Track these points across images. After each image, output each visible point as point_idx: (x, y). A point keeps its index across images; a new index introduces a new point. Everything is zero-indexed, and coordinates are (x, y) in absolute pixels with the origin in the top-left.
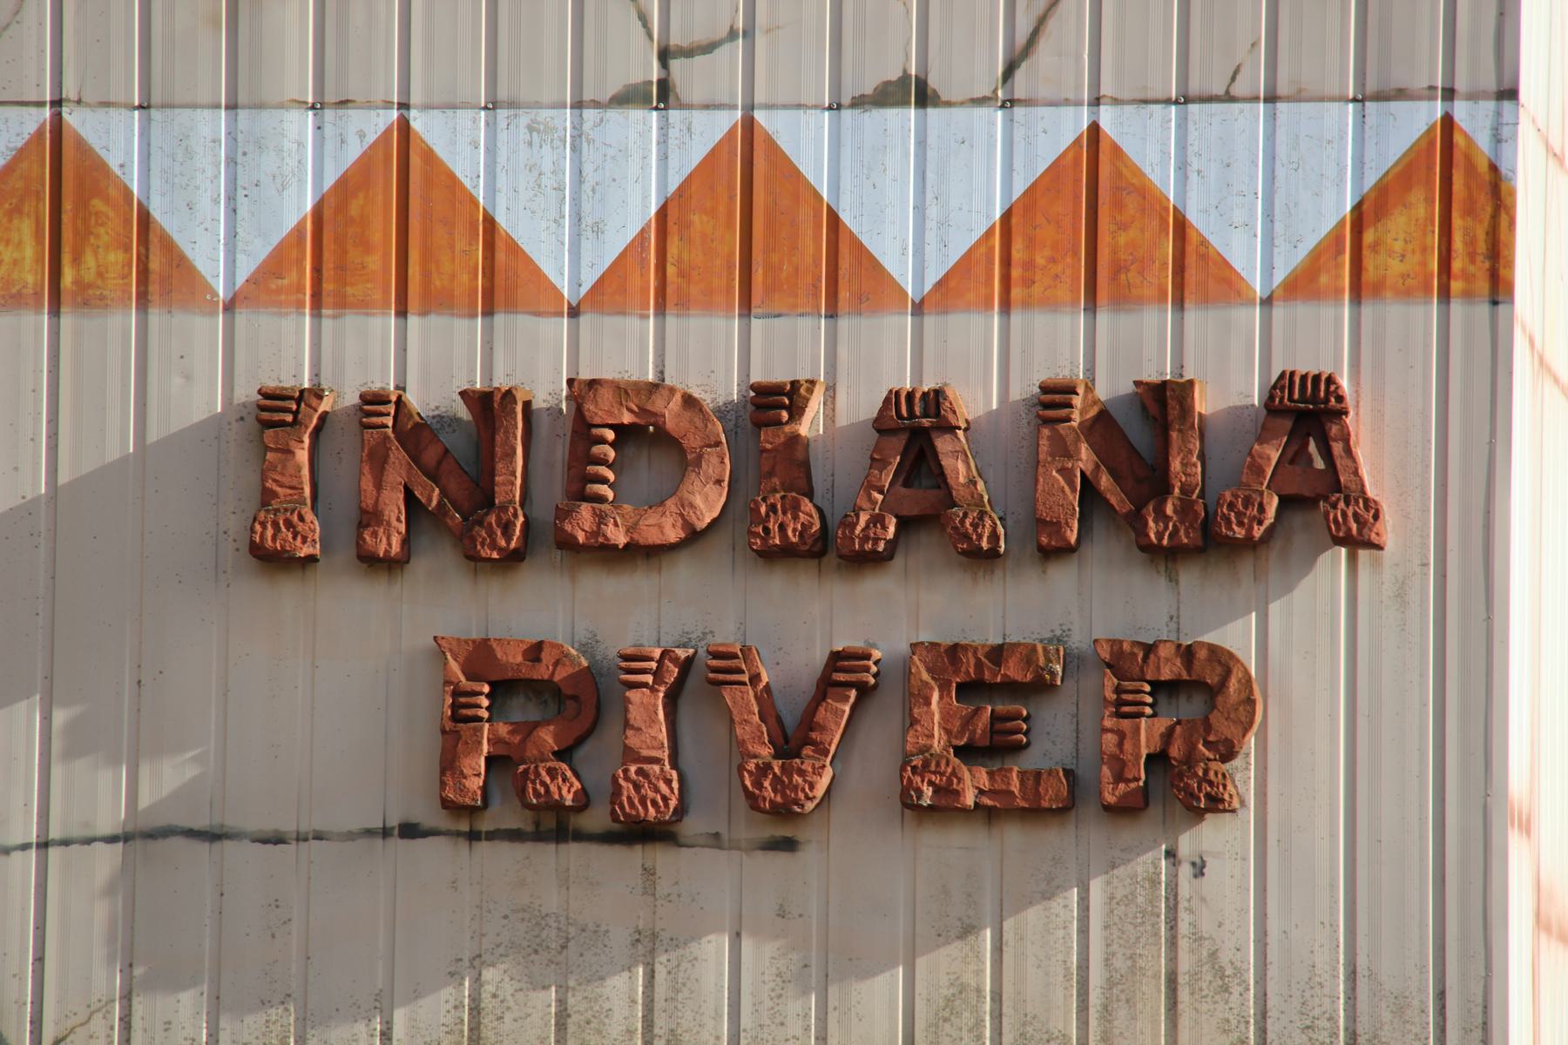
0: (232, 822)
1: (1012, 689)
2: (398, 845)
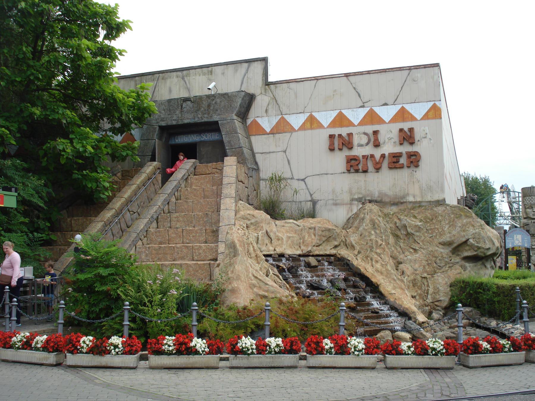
0: (328, 173)
1: (398, 156)
2: (343, 174)
